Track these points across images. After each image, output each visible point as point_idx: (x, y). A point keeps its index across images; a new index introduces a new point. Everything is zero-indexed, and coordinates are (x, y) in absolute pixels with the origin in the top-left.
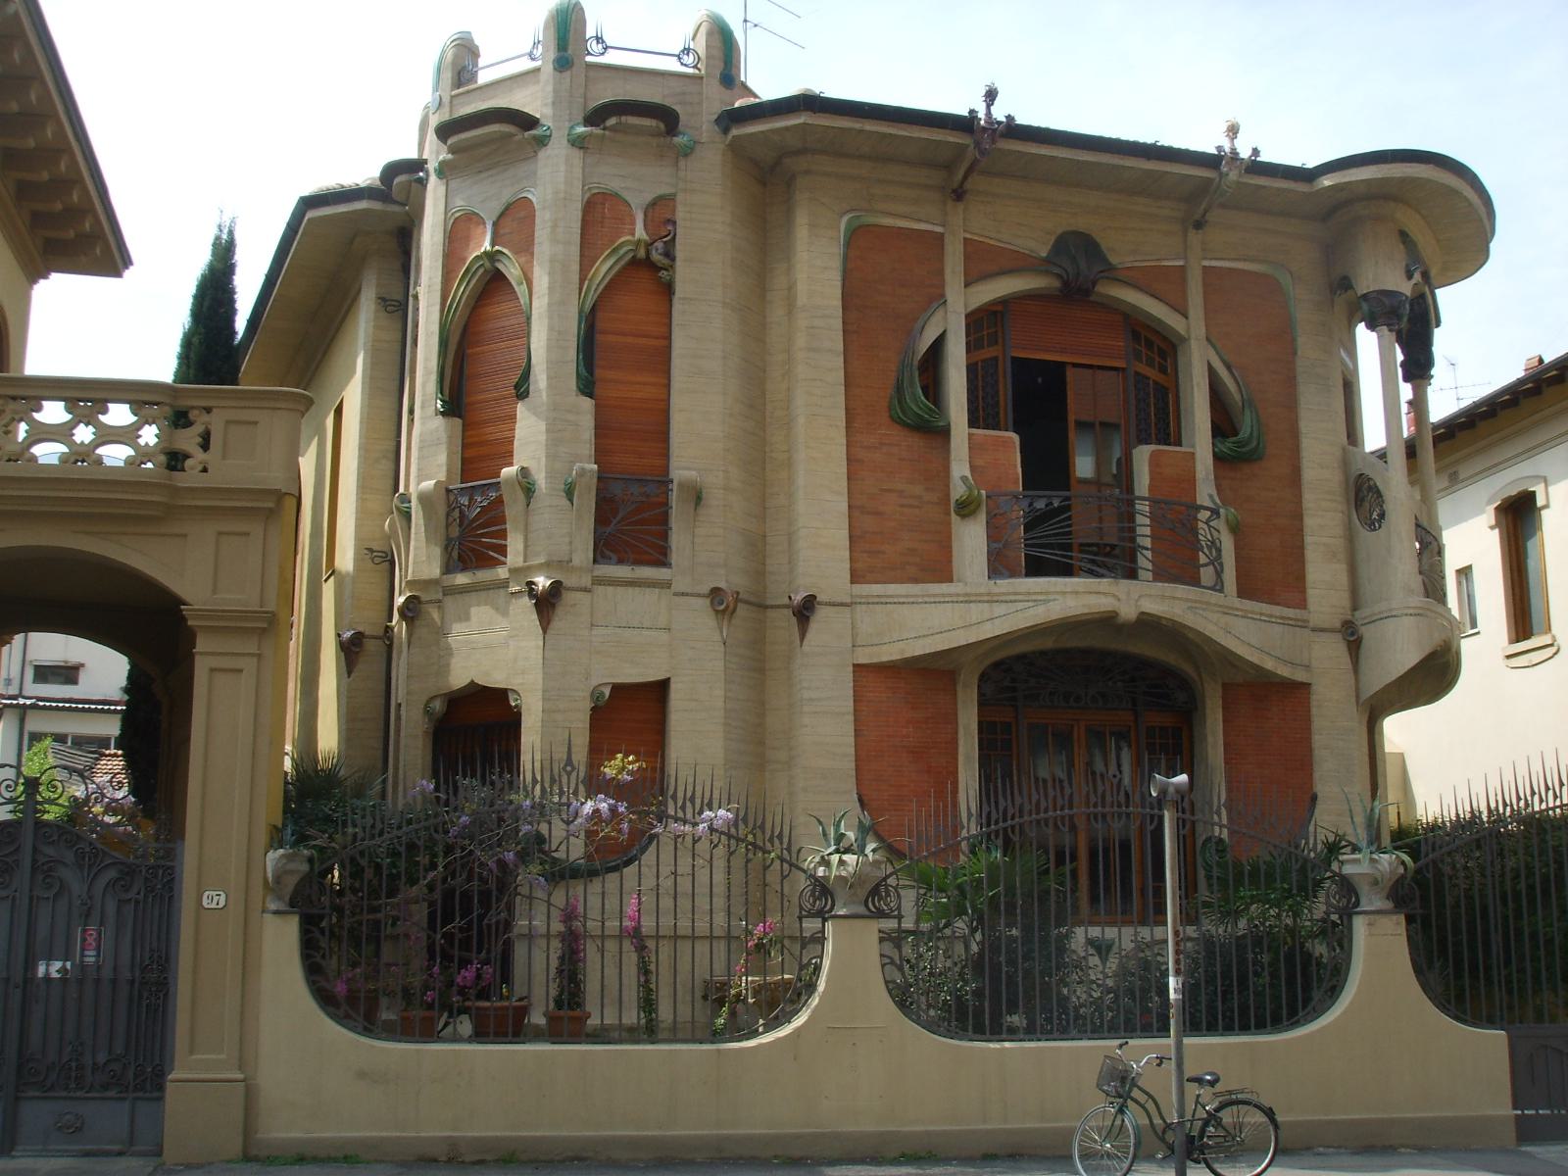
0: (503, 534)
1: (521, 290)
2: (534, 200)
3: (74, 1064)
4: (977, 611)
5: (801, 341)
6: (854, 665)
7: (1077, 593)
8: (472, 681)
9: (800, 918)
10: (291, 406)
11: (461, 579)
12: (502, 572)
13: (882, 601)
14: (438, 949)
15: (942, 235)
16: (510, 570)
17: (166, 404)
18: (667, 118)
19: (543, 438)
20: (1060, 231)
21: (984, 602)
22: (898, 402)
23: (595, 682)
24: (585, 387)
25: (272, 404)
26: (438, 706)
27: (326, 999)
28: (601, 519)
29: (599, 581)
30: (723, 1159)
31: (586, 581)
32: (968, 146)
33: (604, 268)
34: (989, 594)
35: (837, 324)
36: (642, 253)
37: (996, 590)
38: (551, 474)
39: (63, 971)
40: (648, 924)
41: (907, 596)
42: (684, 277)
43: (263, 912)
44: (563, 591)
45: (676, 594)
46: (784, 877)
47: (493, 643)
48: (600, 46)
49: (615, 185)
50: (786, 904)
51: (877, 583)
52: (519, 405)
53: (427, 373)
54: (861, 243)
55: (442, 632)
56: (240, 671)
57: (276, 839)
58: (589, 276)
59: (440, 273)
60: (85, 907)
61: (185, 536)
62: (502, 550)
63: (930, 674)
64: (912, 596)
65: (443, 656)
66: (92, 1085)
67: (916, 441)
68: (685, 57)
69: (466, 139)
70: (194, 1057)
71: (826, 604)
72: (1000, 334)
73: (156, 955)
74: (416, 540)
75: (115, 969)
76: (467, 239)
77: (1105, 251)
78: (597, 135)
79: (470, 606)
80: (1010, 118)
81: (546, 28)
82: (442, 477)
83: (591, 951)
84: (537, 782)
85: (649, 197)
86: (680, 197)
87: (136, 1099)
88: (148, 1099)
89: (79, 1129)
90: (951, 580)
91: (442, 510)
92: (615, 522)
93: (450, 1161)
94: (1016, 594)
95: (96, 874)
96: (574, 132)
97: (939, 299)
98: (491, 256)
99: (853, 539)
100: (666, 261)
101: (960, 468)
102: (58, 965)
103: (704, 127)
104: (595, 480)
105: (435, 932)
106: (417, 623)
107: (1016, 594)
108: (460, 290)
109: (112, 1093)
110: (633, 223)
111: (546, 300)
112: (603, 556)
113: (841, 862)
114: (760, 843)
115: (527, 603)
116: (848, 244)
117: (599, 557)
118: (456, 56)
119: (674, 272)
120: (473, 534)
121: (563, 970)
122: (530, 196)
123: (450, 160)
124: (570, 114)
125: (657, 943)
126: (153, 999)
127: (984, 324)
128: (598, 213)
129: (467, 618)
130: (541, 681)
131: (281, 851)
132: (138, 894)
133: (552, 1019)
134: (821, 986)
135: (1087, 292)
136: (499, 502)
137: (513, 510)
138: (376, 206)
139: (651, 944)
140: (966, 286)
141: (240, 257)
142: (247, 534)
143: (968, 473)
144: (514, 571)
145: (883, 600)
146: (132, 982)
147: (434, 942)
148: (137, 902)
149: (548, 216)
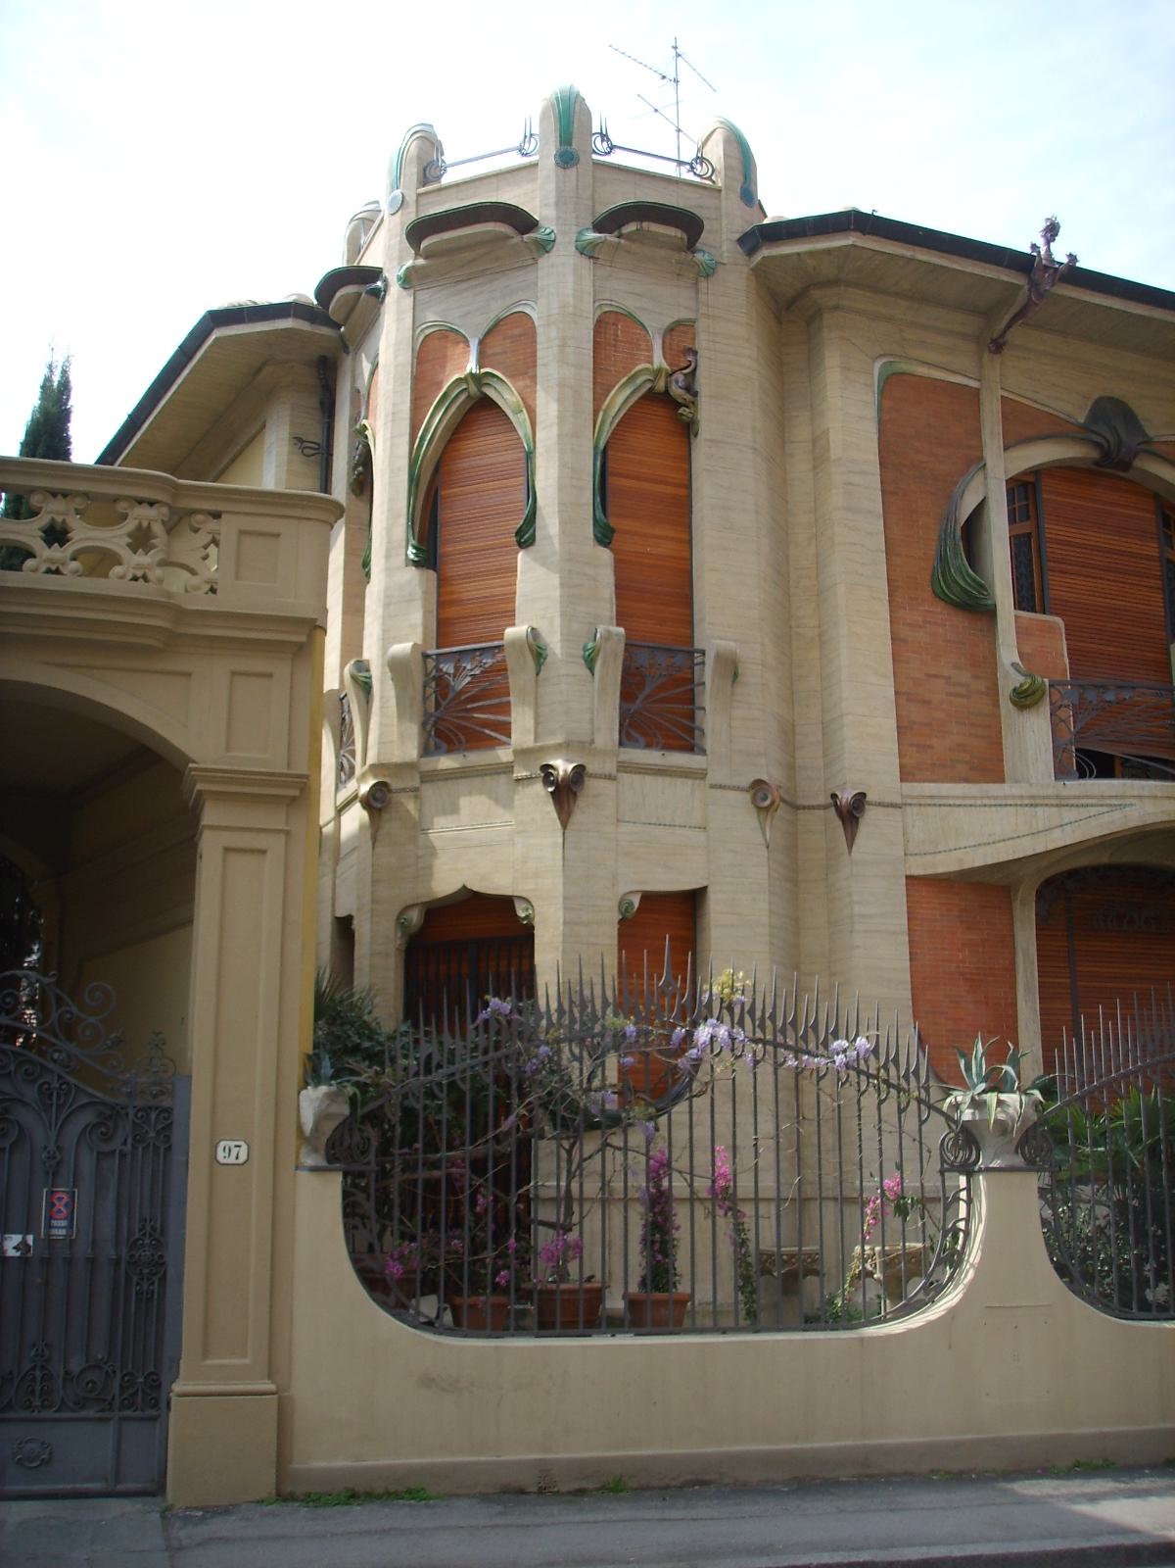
0: (505, 708)
1: (521, 421)
2: (534, 315)
3: (38, 1374)
4: (1043, 816)
5: (836, 498)
6: (907, 877)
7: (1155, 797)
8: (464, 887)
9: (942, 1172)
10: (323, 518)
11: (446, 762)
12: (504, 755)
13: (933, 802)
14: (512, 1216)
15: (978, 390)
16: (516, 752)
17: (165, 504)
18: (690, 225)
19: (550, 595)
20: (1096, 396)
21: (1052, 805)
22: (942, 580)
23: (623, 889)
24: (603, 534)
25: (298, 513)
26: (415, 917)
27: (373, 1282)
28: (627, 695)
29: (625, 768)
30: (871, 1476)
31: (610, 767)
32: (1021, 287)
33: (619, 399)
34: (1057, 797)
35: (876, 481)
36: (661, 385)
37: (1065, 792)
38: (567, 638)
39: (23, 1246)
40: (745, 1186)
41: (964, 798)
42: (710, 416)
43: (297, 1168)
44: (586, 779)
45: (713, 787)
46: (922, 1123)
47: (489, 839)
48: (605, 144)
49: (629, 304)
50: (925, 1154)
51: (925, 781)
52: (520, 555)
53: (392, 515)
54: (894, 388)
55: (419, 828)
56: (263, 852)
57: (313, 1074)
58: (604, 407)
59: (409, 398)
60: (54, 1162)
61: (188, 675)
62: (505, 729)
63: (983, 889)
64: (970, 798)
65: (423, 858)
66: (63, 1402)
67: (960, 622)
68: (698, 167)
69: (448, 241)
70: (209, 1362)
71: (881, 804)
72: (1031, 508)
73: (148, 1228)
74: (382, 715)
75: (94, 1244)
76: (443, 360)
77: (1143, 423)
78: (611, 244)
79: (458, 797)
80: (1073, 258)
81: (544, 117)
82: (418, 637)
83: (681, 1215)
84: (565, 1013)
85: (668, 321)
86: (701, 325)
87: (122, 1419)
88: (141, 1419)
89: (45, 1463)
90: (1002, 780)
91: (418, 678)
92: (641, 697)
93: (541, 1491)
94: (1087, 797)
95: (66, 1119)
96: (584, 238)
97: (975, 462)
98: (477, 379)
99: (901, 730)
100: (688, 397)
101: (1008, 653)
102: (16, 1239)
103: (724, 248)
104: (622, 646)
105: (507, 1192)
106: (385, 816)
107: (1087, 797)
108: (436, 420)
109: (91, 1413)
110: (650, 349)
111: (555, 431)
112: (629, 737)
113: (1000, 1103)
114: (894, 1081)
115: (540, 792)
116: (882, 393)
117: (625, 740)
118: (420, 150)
119: (696, 411)
120: (459, 707)
121: (653, 1243)
122: (527, 310)
123: (422, 267)
124: (577, 218)
125: (757, 1209)
126: (145, 1286)
127: (1024, 490)
128: (612, 333)
129: (454, 810)
130: (561, 888)
131: (323, 1089)
132: (125, 1143)
133: (633, 1304)
134: (974, 1255)
135: (1126, 466)
136: (501, 669)
137: (519, 679)
138: (303, 325)
139: (748, 1209)
140: (1005, 449)
141: (78, 403)
142: (270, 676)
143: (1017, 660)
144: (522, 753)
145: (937, 801)
146: (117, 1262)
147: (506, 1208)
148: (123, 1155)
149: (553, 333)
